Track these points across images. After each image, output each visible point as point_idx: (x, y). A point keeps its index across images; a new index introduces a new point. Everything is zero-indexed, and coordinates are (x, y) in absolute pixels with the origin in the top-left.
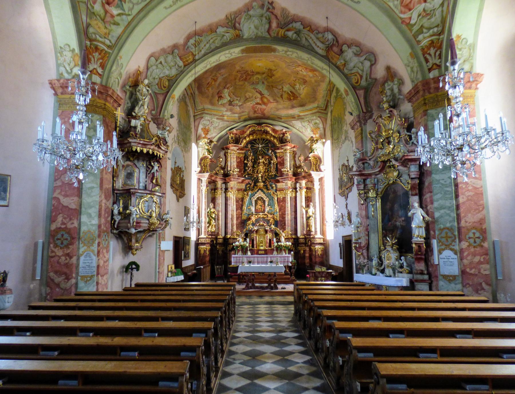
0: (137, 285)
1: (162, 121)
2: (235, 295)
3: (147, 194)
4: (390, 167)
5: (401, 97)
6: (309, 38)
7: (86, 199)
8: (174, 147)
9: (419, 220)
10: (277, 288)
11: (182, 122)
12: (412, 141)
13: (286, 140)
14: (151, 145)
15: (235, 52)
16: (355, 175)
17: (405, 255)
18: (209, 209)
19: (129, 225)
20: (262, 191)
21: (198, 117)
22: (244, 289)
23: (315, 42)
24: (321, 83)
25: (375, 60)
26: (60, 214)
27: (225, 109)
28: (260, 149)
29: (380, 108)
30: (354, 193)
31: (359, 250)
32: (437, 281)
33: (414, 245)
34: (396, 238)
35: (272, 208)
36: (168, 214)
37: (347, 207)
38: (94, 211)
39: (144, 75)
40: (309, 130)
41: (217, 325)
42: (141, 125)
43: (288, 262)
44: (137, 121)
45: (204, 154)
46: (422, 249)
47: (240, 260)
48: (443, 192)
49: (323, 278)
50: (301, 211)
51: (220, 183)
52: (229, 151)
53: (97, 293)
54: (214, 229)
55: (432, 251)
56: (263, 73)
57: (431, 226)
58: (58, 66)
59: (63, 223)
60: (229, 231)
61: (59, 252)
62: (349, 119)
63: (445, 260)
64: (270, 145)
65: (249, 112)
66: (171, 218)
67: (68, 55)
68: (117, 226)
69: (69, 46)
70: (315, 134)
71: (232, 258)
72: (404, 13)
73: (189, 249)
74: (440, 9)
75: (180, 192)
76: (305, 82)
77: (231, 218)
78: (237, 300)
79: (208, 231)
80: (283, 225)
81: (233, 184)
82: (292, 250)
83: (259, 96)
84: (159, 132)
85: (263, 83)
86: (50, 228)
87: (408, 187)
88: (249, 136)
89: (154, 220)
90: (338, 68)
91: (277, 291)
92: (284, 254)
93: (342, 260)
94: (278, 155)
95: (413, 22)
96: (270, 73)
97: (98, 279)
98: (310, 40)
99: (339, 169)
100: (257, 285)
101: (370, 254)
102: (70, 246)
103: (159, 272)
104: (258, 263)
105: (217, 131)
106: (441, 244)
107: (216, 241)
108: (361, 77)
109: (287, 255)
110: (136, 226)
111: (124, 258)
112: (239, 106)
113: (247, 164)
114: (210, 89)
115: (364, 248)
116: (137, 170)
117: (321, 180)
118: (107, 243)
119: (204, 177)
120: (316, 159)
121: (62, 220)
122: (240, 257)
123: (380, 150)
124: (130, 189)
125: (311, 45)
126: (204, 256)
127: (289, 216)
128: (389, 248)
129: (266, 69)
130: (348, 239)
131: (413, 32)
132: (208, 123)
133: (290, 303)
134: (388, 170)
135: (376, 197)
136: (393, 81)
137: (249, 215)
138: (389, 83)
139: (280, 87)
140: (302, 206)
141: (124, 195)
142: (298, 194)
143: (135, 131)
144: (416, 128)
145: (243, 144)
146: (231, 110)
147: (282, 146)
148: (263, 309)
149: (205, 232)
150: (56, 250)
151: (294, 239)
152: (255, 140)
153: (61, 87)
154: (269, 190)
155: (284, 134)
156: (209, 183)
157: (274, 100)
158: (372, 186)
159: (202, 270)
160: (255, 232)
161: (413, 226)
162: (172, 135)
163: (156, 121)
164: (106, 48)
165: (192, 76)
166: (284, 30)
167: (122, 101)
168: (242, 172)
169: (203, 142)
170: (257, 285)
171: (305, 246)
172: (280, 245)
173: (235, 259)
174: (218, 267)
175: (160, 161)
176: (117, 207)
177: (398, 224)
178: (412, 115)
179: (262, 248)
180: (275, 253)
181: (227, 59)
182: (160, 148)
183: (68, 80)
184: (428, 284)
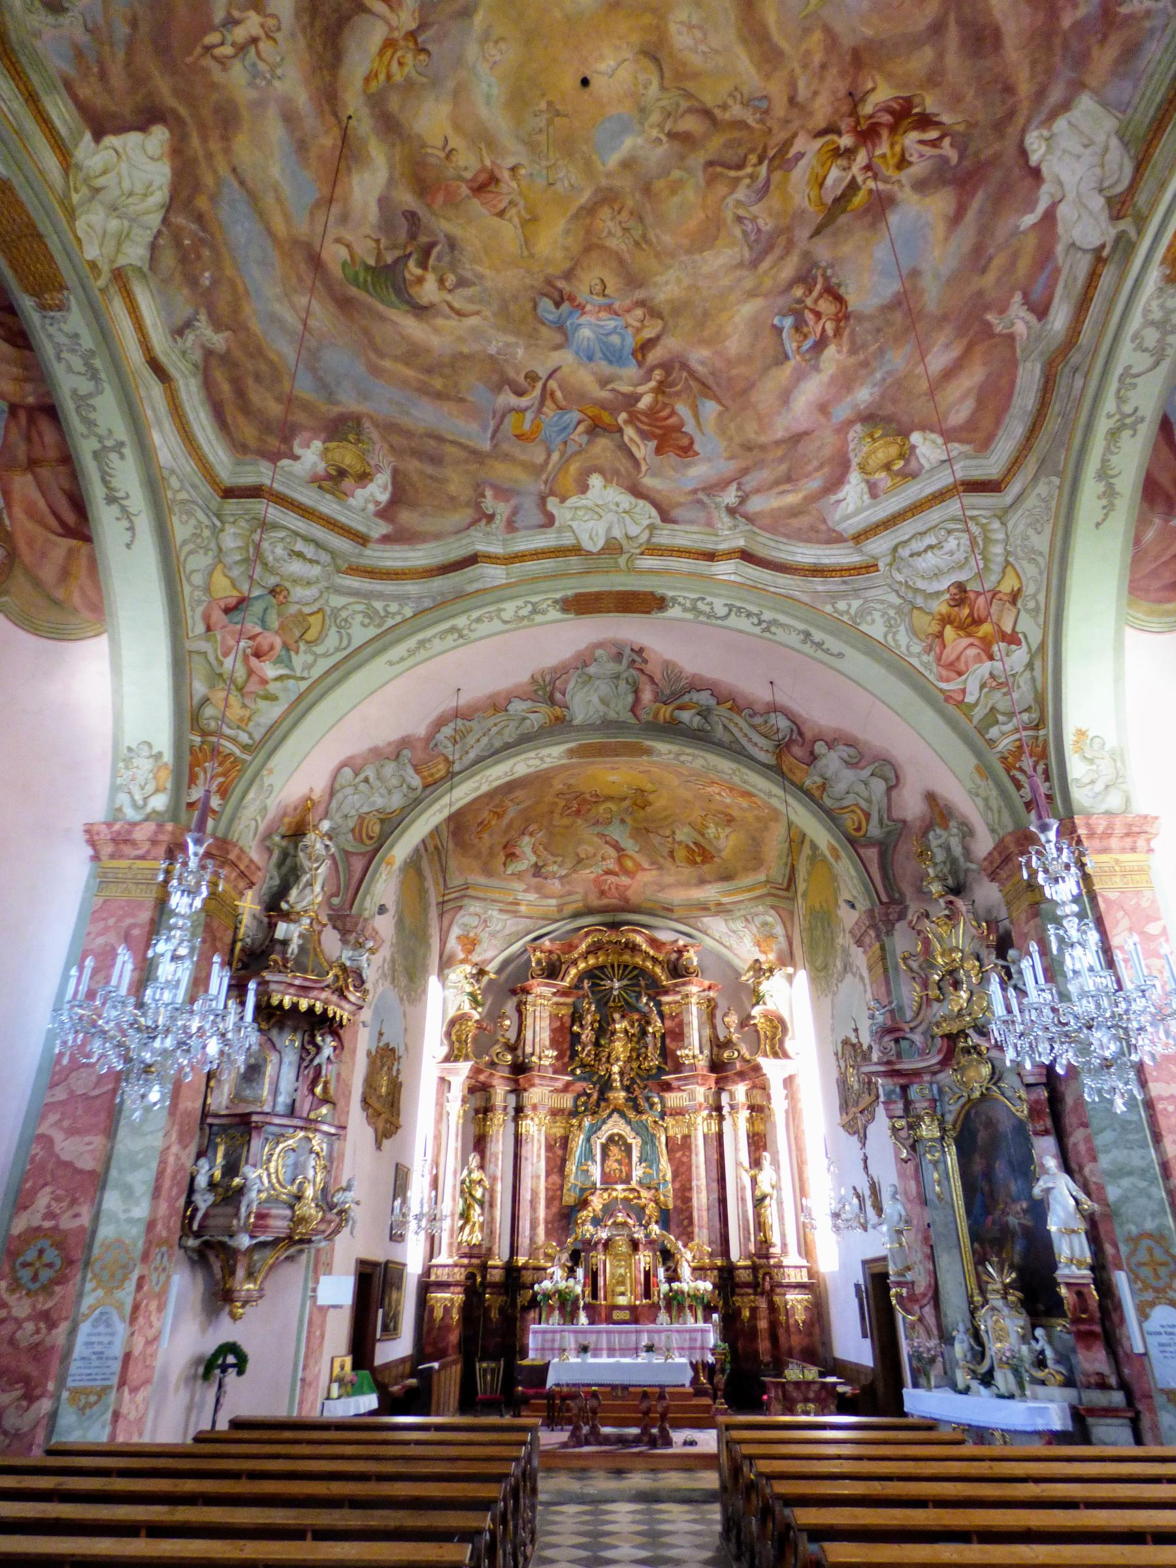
0: (236, 1424)
1: (356, 924)
2: (535, 1463)
3: (296, 1127)
4: (967, 1051)
5: (973, 866)
6: (731, 726)
7: (126, 1143)
8: (380, 989)
9: (1065, 1208)
10: (668, 1443)
11: (408, 921)
12: (1013, 982)
13: (687, 969)
14: (323, 989)
15: (552, 755)
16: (877, 1074)
17: (1044, 1321)
18: (465, 1172)
19: (235, 1222)
20: (623, 1115)
21: (449, 907)
22: (564, 1445)
23: (746, 735)
24: (772, 824)
25: (897, 777)
26: (45, 1185)
27: (522, 886)
28: (615, 993)
29: (923, 894)
30: (880, 1128)
31: (909, 1305)
32: (1152, 1410)
33: (1063, 1291)
34: (1012, 1267)
35: (650, 1167)
36: (348, 1188)
37: (866, 1167)
38: (141, 1180)
39: (321, 810)
40: (748, 942)
41: (479, 1558)
42: (301, 936)
43: (702, 1348)
44: (292, 926)
45: (459, 1009)
46: (1090, 1302)
47: (553, 1340)
48: (1117, 1126)
49: (811, 1406)
50: (738, 1177)
51: (500, 1093)
52: (530, 998)
53: (113, 1448)
54: (477, 1238)
55: (1119, 1307)
56: (624, 799)
57: (1102, 1228)
58: (115, 789)
59: (50, 1215)
60: (524, 1242)
61: (21, 1308)
62: (849, 918)
63: (1164, 1339)
64: (642, 983)
65: (586, 895)
66: (358, 1203)
67: (144, 766)
68: (200, 1226)
69: (150, 745)
70: (765, 953)
71: (531, 1336)
72: (948, 680)
73: (398, 1302)
74: (1028, 674)
75: (387, 1121)
76: (730, 820)
77: (532, 1201)
78: (541, 1485)
79: (460, 1243)
80: (685, 1222)
81: (538, 1094)
82: (715, 1309)
83: (613, 853)
84: (346, 956)
85: (623, 821)
86: (8, 1230)
87: (1023, 1111)
88: (585, 956)
89: (308, 1208)
90: (808, 793)
91: (670, 1451)
92: (690, 1323)
93: (868, 1341)
94: (666, 1009)
95: (970, 699)
96: (640, 800)
97: (119, 1401)
98: (735, 730)
99: (836, 1054)
100: (606, 1430)
101: (944, 1321)
102: (57, 1289)
103: (303, 1380)
104: (611, 1352)
105: (498, 943)
106: (1139, 1285)
107: (484, 1277)
108: (868, 816)
109: (701, 1325)
110: (255, 1226)
111: (204, 1330)
112: (561, 878)
113: (578, 1035)
114: (485, 836)
115: (925, 1301)
116: (273, 1058)
117: (789, 1082)
118: (163, 1278)
119: (455, 1072)
120: (771, 1021)
121: (48, 1206)
122: (554, 1332)
123: (936, 1005)
124: (250, 1114)
125: (737, 741)
126: (445, 1328)
127: (704, 1195)
128: (996, 1300)
129: (630, 788)
130: (878, 1269)
131: (975, 721)
132: (474, 921)
133: (708, 1497)
134: (964, 1060)
135: (942, 1138)
136: (946, 828)
137: (583, 1190)
138: (939, 831)
139: (668, 833)
140: (738, 1164)
141: (231, 1131)
142: (727, 1125)
143: (284, 952)
144: (1020, 949)
145: (568, 979)
146: (538, 889)
147: (676, 985)
148: (623, 1515)
149: (451, 1245)
150: (12, 1300)
151: (720, 1269)
152: (601, 968)
153: (113, 840)
154: (640, 1112)
155: (680, 952)
156: (472, 1090)
157: (652, 863)
158: (926, 1104)
159: (435, 1377)
160: (600, 1247)
161: (1053, 1228)
162: (377, 959)
163: (339, 924)
164: (237, 752)
165: (440, 811)
166: (671, 708)
167: (260, 874)
168: (566, 1059)
169: (460, 974)
170: (606, 1430)
171: (755, 1294)
172: (676, 1292)
173: (540, 1336)
174: (484, 1365)
175: (341, 1032)
176: (207, 1167)
177: (1012, 1221)
178: (1003, 913)
179: (622, 1301)
180: (663, 1316)
181: (532, 770)
182: (345, 998)
183: (134, 824)
184: (1126, 1421)
